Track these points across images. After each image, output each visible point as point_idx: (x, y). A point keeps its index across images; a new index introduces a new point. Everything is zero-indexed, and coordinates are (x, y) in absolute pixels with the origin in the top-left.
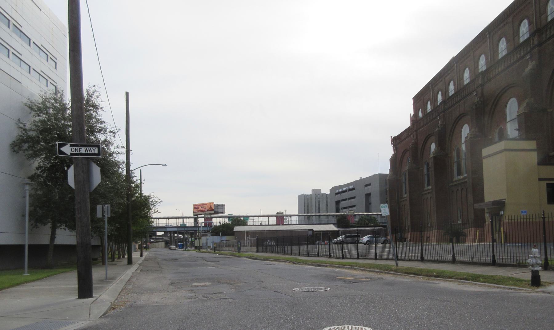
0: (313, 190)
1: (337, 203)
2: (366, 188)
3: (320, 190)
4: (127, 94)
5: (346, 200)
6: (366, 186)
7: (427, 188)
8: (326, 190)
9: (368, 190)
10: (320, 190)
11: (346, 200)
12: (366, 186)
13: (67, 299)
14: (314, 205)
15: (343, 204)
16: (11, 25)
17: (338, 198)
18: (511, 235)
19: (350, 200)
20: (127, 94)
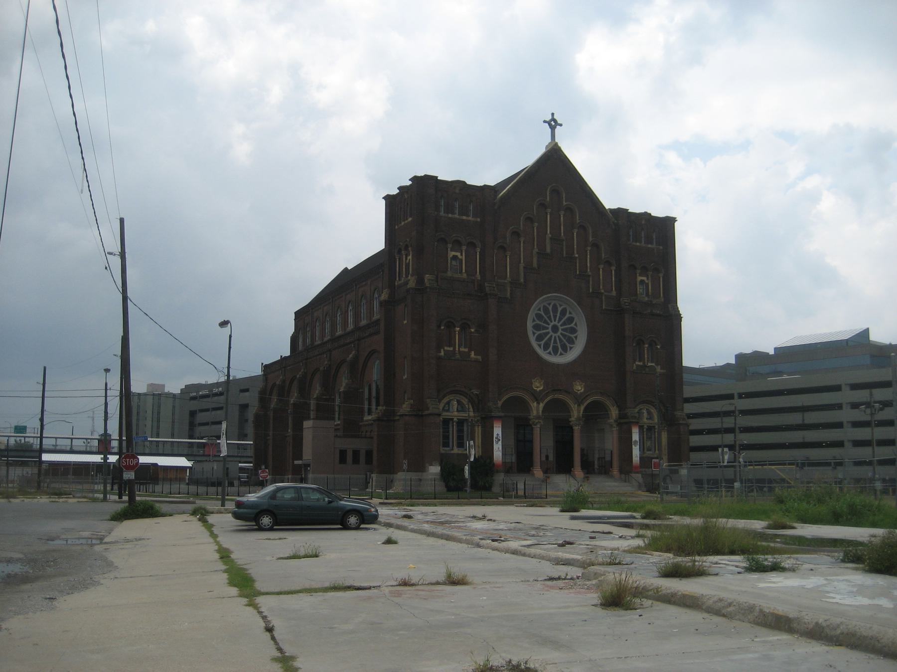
0: (151, 385)
1: (193, 414)
2: (242, 394)
3: (164, 386)
4: (122, 221)
5: (207, 410)
6: (243, 391)
7: (367, 418)
8: (174, 387)
9: (245, 398)
10: (164, 386)
11: (207, 410)
12: (243, 391)
13: (148, 499)
14: (149, 412)
15: (201, 417)
16: (628, 558)
17: (195, 405)
18: (812, 418)
19: (213, 413)
20: (122, 221)
